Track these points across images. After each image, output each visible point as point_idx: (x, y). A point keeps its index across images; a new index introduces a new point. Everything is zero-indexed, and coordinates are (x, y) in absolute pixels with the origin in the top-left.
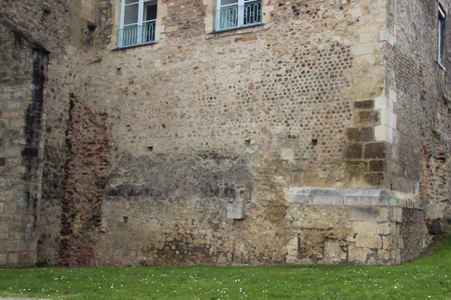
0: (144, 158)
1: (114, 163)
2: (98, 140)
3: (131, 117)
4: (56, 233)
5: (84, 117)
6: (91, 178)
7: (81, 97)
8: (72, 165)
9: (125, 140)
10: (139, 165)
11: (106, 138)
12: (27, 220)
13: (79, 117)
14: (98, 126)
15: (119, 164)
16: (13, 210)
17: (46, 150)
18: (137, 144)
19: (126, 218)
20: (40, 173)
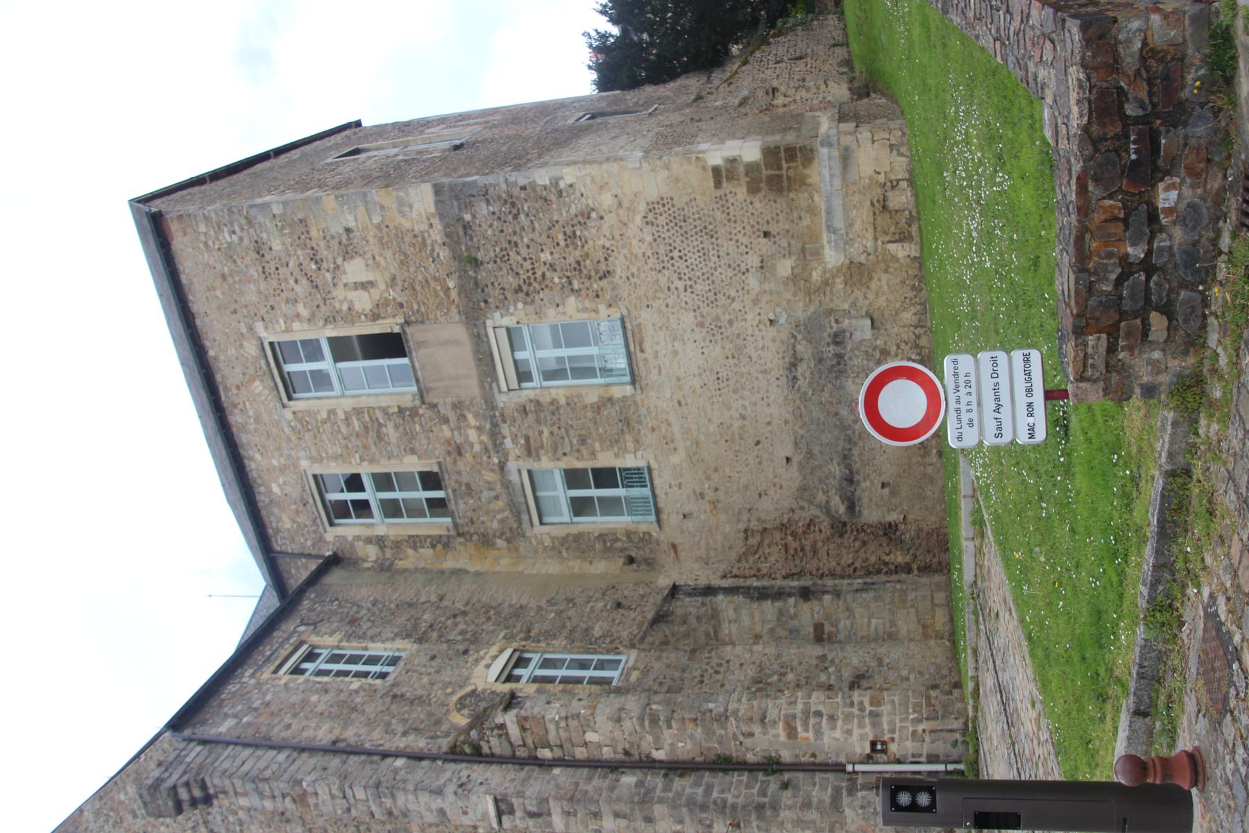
0: (802, 467)
19: (883, 485)
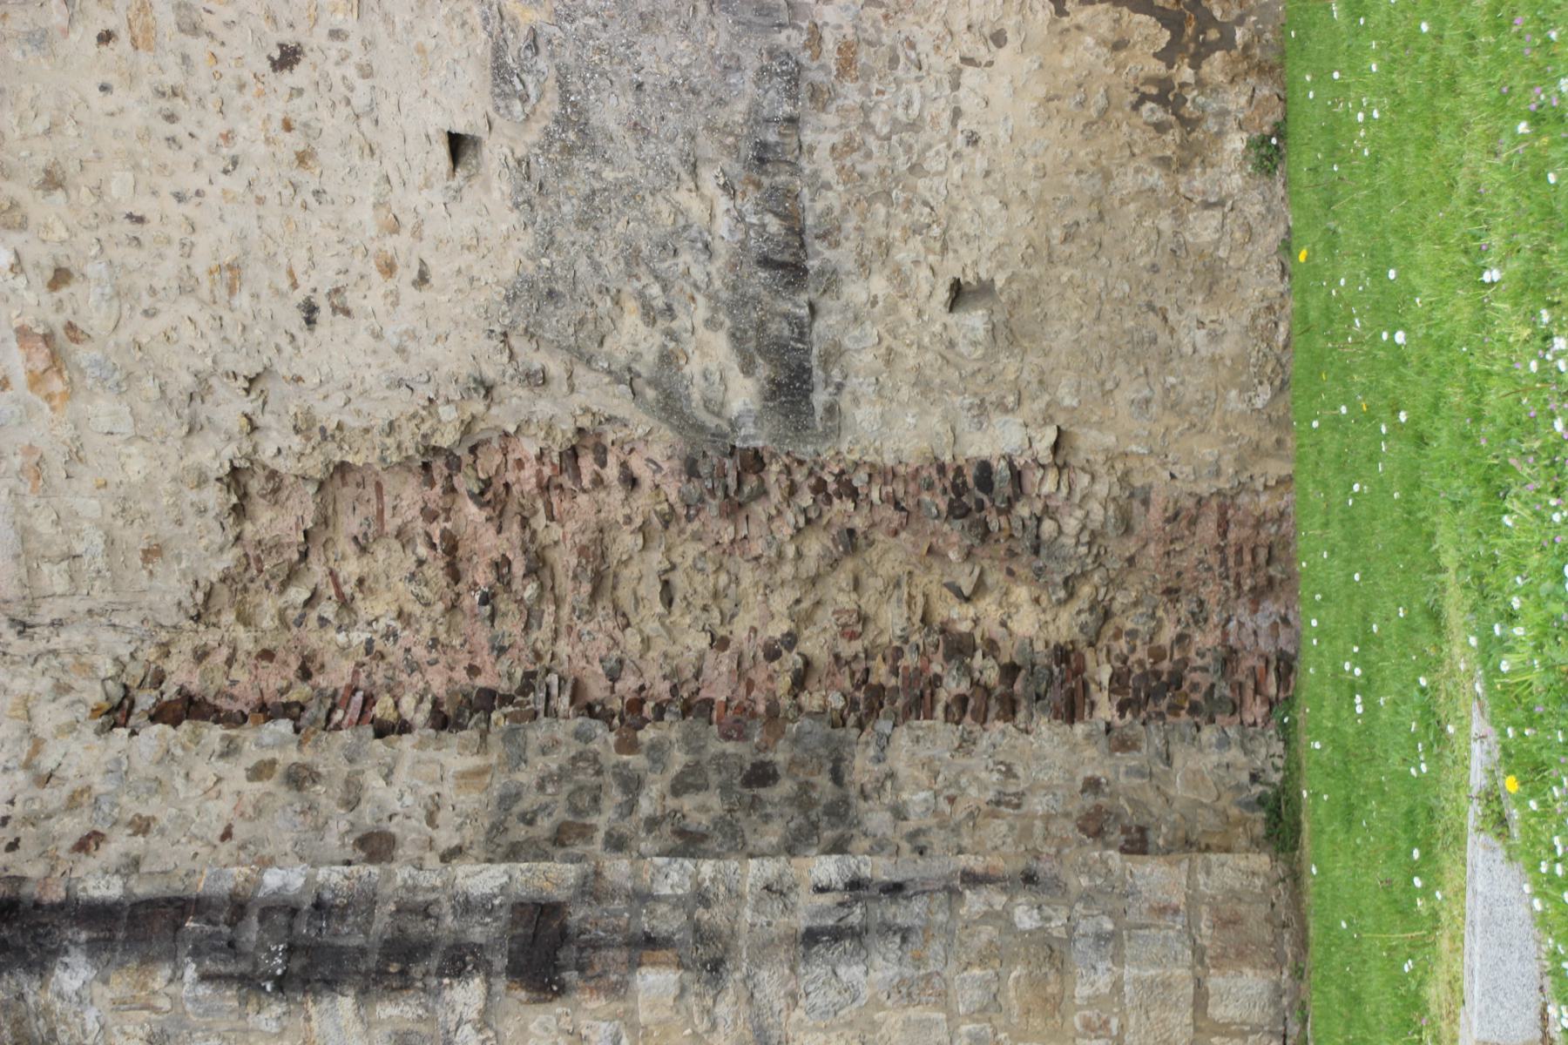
0: (531, 190)
1: (578, 399)
2: (430, 515)
3: (243, 300)
4: (1074, 748)
5: (268, 622)
6: (692, 550)
7: (124, 652)
8: (613, 676)
9: (413, 335)
10: (583, 222)
11: (406, 463)
12: (987, 932)
13: (267, 655)
14: (324, 521)
15: (589, 361)
16: (925, 1026)
17: (514, 853)
18: (439, 243)
19: (959, 295)
20: (673, 877)
